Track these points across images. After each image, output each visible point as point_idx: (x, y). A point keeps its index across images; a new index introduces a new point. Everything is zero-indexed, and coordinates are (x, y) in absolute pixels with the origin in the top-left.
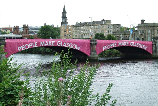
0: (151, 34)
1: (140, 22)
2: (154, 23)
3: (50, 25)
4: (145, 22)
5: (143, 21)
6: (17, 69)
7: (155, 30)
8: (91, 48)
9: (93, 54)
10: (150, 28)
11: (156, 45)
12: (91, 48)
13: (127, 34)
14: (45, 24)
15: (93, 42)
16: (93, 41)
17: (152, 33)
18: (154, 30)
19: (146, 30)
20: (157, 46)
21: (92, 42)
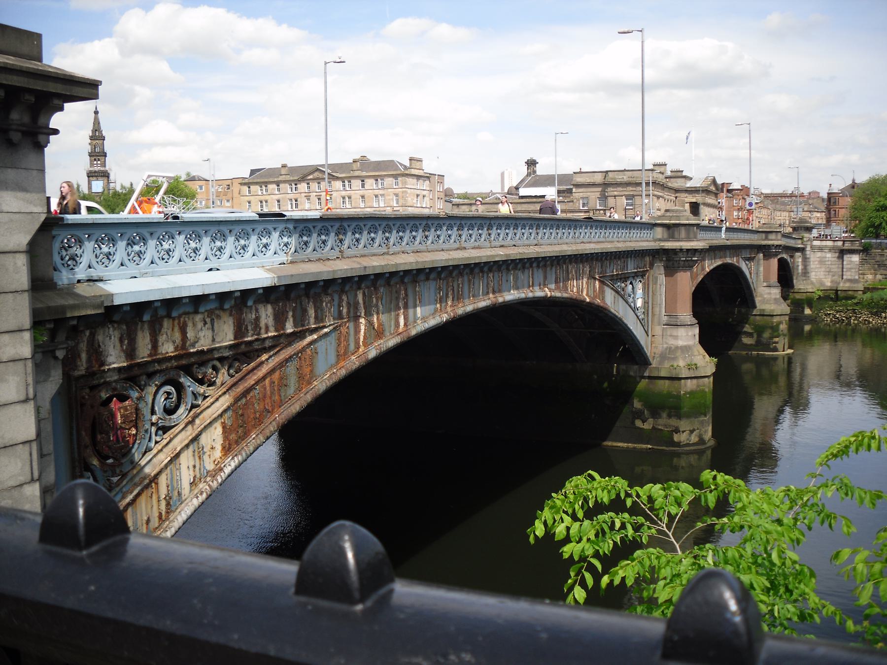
4: (540, 170)
19: (615, 196)
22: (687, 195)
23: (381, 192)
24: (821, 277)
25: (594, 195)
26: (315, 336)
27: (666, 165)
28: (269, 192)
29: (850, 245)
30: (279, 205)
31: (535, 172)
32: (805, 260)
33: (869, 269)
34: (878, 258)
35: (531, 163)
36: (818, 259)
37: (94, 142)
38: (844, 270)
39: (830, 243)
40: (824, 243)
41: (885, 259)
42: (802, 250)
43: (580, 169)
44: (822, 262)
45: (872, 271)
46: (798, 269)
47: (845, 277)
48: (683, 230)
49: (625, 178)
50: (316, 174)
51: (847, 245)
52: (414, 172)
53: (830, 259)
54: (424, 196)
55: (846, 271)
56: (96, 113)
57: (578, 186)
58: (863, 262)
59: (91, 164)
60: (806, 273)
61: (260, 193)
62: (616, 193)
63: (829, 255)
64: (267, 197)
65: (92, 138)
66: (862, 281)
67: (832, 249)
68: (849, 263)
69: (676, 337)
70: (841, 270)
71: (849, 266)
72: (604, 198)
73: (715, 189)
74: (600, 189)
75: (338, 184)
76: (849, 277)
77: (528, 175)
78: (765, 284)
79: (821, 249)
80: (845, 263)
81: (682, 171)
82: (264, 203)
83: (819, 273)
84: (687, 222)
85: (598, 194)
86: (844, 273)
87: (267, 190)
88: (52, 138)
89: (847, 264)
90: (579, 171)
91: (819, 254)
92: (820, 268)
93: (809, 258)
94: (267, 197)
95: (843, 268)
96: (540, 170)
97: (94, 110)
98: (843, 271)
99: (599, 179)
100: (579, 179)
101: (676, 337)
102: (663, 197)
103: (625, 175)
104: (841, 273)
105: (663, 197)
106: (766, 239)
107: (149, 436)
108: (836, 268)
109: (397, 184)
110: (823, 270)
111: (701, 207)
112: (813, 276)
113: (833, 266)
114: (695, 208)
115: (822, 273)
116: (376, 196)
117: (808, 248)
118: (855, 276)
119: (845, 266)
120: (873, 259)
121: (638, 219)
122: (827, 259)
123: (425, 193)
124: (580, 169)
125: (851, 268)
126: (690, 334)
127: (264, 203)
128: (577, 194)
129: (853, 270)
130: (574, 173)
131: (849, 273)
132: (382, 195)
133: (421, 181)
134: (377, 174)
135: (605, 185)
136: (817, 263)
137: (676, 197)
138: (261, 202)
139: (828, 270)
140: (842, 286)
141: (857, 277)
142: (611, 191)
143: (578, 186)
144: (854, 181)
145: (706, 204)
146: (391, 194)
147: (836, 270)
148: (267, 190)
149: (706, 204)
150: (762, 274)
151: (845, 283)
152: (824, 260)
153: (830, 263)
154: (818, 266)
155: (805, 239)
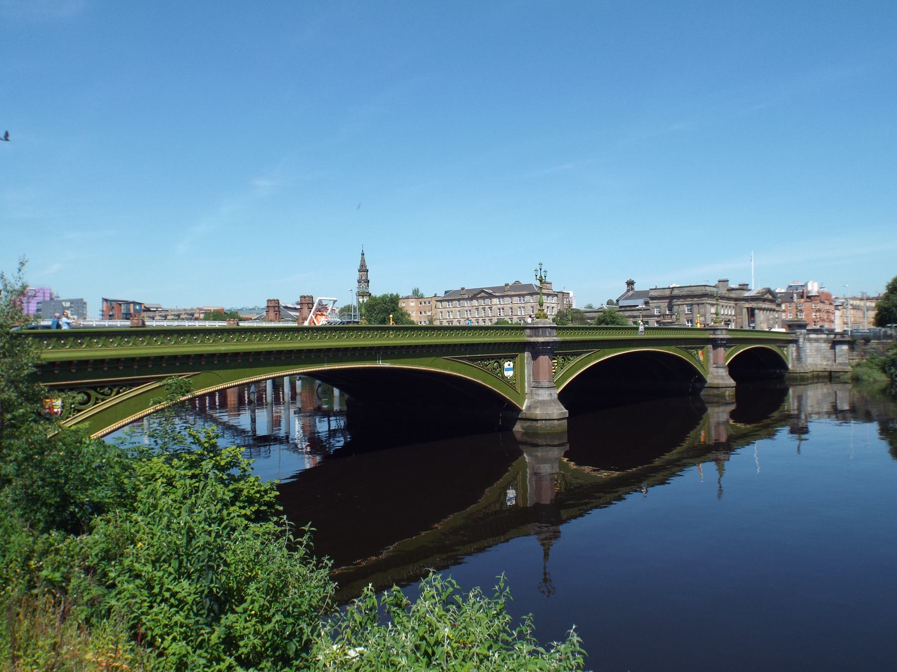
4: (637, 287)
19: (679, 305)
22: (743, 302)
23: (523, 305)
25: (664, 304)
26: (157, 385)
27: (728, 281)
28: (454, 306)
30: (512, 312)
31: (632, 289)
32: (798, 348)
33: (857, 356)
35: (630, 283)
37: (361, 273)
38: (837, 356)
39: (824, 336)
42: (795, 342)
44: (818, 350)
47: (837, 361)
48: (541, 330)
49: (684, 292)
50: (483, 294)
52: (544, 291)
54: (553, 308)
56: (363, 254)
57: (653, 298)
59: (119, 303)
61: (498, 303)
62: (679, 303)
63: (824, 345)
64: (453, 309)
65: (360, 271)
67: (826, 341)
69: (538, 395)
70: (833, 356)
71: (840, 353)
72: (670, 308)
73: (769, 297)
74: (668, 301)
75: (495, 301)
76: (841, 362)
77: (628, 291)
78: (715, 366)
79: (817, 340)
80: (837, 351)
81: (747, 285)
82: (502, 310)
84: (543, 326)
85: (666, 304)
86: (837, 359)
87: (524, 300)
90: (654, 288)
91: (815, 344)
94: (453, 309)
95: (835, 355)
96: (637, 287)
97: (361, 252)
98: (835, 357)
99: (668, 293)
100: (653, 294)
101: (538, 395)
104: (833, 359)
106: (714, 334)
107: (80, 426)
108: (830, 354)
109: (520, 300)
110: (819, 356)
111: (756, 311)
112: (810, 360)
113: (827, 353)
114: (751, 312)
115: (819, 359)
116: (520, 308)
117: (801, 340)
119: (837, 353)
121: (306, 324)
123: (553, 305)
125: (842, 355)
126: (547, 393)
127: (502, 310)
128: (652, 304)
129: (844, 356)
130: (651, 289)
131: (840, 359)
132: (524, 307)
133: (550, 297)
134: (520, 293)
135: (671, 298)
136: (813, 351)
137: (736, 304)
138: (500, 309)
139: (823, 356)
140: (835, 368)
142: (675, 302)
143: (653, 298)
145: (760, 309)
146: (529, 307)
147: (830, 356)
148: (524, 300)
149: (760, 309)
151: (837, 366)
154: (815, 353)
155: (798, 333)
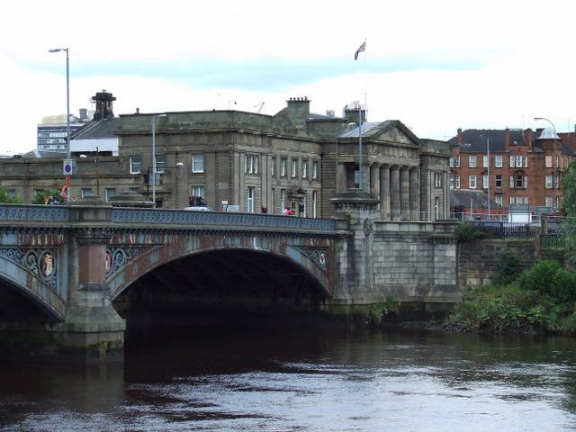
0: (210, 177)
1: (92, 108)
2: (231, 113)
3: (455, 134)
4: (118, 109)
5: (104, 99)
6: (565, 384)
7: (237, 155)
8: (76, 263)
9: (94, 309)
10: (204, 139)
11: (357, 242)
12: (76, 263)
13: (47, 178)
14: (459, 130)
15: (90, 225)
16: (90, 216)
17: (217, 171)
18: (230, 153)
19: (177, 153)
20: (357, 248)
21: (83, 224)
24: (401, 282)
29: (442, 231)
34: (484, 253)
36: (395, 254)
40: (405, 228)
41: (494, 253)
43: (138, 110)
45: (477, 272)
46: (339, 269)
51: (438, 231)
53: (415, 253)
55: (439, 273)
58: (462, 257)
60: (353, 274)
63: (413, 247)
66: (463, 287)
68: (441, 259)
71: (442, 265)
76: (443, 283)
83: (397, 276)
88: (114, 102)
89: (439, 262)
90: (134, 112)
92: (400, 267)
93: (359, 252)
102: (170, 153)
103: (192, 120)
105: (170, 153)
110: (404, 270)
113: (419, 265)
118: (451, 280)
120: (478, 254)
122: (411, 254)
124: (138, 110)
125: (445, 268)
131: (442, 276)
136: (393, 259)
139: (412, 270)
140: (433, 296)
141: (454, 283)
144: (115, 99)
150: (77, 272)
152: (406, 254)
153: (415, 259)
